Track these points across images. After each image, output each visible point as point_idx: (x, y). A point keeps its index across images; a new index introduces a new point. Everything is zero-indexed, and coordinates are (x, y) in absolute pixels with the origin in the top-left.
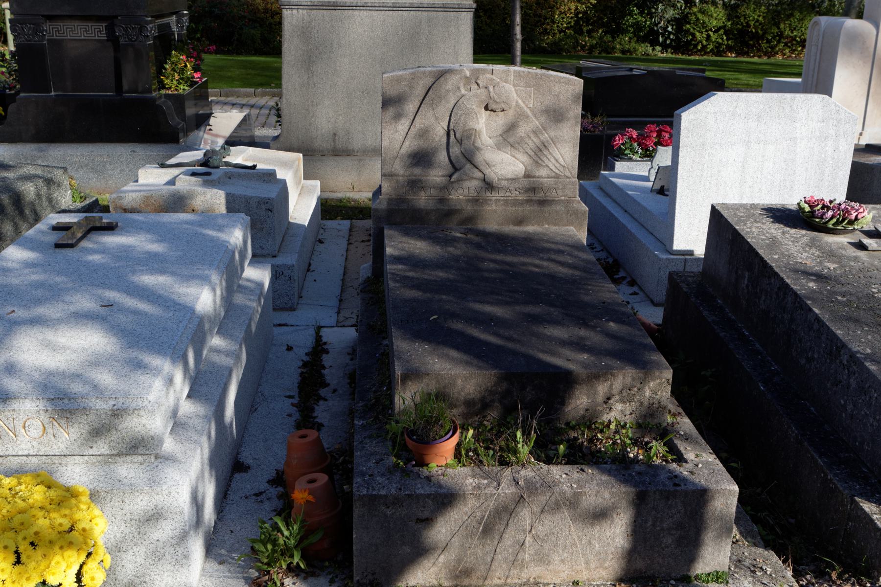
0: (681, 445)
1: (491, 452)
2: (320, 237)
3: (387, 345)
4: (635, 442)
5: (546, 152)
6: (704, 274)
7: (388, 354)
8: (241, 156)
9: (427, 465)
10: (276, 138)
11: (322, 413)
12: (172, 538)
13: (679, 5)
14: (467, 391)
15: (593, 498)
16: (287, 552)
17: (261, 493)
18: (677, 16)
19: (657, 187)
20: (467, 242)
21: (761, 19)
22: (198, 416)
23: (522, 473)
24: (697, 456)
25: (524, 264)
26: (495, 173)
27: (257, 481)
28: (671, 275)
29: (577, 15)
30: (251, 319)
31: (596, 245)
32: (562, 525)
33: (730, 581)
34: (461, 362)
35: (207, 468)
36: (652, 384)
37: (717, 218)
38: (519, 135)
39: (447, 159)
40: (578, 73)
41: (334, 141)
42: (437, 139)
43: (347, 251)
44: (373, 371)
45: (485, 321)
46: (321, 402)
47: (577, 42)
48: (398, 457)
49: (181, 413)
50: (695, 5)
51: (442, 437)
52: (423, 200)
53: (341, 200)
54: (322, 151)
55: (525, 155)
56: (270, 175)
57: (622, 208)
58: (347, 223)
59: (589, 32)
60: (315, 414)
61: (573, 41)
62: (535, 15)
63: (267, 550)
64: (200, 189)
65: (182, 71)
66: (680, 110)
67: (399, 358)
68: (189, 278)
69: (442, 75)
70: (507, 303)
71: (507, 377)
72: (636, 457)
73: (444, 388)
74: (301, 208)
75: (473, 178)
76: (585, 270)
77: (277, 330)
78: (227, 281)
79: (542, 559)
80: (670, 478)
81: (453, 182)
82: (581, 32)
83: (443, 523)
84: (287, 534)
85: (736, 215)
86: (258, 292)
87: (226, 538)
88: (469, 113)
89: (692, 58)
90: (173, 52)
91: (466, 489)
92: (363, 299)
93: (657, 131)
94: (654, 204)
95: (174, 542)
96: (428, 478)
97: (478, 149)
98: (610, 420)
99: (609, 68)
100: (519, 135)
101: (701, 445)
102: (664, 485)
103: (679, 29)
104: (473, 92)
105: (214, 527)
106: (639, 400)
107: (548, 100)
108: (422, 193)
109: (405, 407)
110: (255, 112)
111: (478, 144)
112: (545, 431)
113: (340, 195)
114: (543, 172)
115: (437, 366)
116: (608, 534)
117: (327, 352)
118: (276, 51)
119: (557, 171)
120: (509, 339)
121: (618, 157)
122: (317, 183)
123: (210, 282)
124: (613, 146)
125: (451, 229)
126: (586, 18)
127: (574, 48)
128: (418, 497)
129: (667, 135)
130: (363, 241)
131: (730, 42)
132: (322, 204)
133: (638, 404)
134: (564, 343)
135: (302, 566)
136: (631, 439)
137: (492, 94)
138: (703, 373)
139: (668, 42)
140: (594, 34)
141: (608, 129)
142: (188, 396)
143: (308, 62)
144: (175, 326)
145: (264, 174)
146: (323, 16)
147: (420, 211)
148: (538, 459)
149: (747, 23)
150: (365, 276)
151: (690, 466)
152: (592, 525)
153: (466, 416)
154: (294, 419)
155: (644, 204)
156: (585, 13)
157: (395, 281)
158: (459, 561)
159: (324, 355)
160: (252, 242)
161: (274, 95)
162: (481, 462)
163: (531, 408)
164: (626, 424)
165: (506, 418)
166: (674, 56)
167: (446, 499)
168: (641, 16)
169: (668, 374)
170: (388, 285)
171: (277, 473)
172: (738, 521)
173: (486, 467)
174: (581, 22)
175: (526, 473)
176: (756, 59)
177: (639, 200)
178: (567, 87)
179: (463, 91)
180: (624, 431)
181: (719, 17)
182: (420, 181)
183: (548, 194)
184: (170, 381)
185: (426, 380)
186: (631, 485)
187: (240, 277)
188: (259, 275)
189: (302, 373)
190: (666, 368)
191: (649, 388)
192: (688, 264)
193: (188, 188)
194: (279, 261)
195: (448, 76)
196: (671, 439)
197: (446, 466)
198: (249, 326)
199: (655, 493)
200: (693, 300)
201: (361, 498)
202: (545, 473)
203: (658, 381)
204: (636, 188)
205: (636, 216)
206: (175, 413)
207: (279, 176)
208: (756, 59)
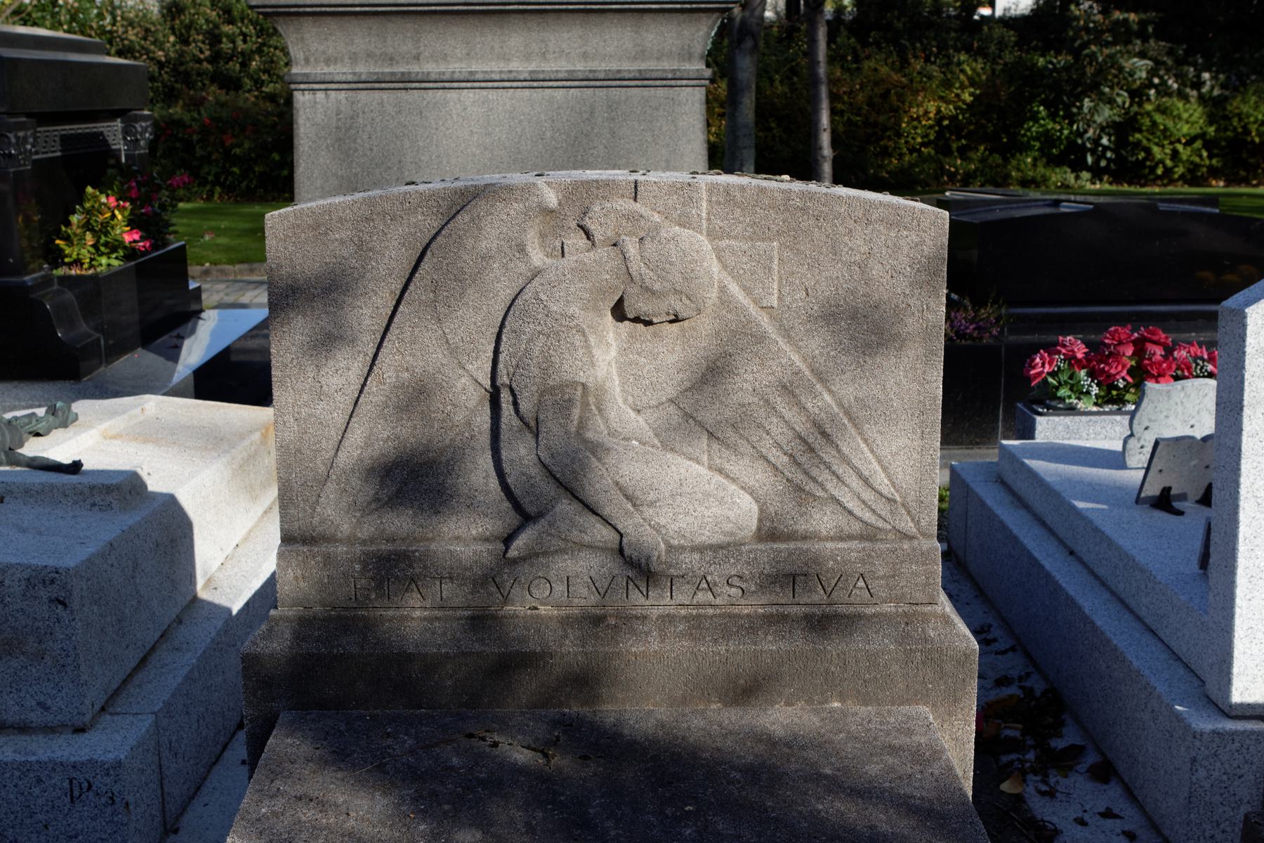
5: (828, 455)
13: (1119, 100)
18: (1117, 119)
19: (1152, 490)
26: (657, 528)
29: (939, 121)
31: (996, 632)
38: (736, 398)
39: (494, 483)
40: (941, 204)
42: (459, 417)
50: (1148, 100)
52: (415, 617)
55: (760, 465)
56: (125, 489)
57: (1061, 542)
59: (963, 152)
61: (934, 166)
65: (105, 228)
69: (463, 202)
75: (583, 546)
81: (514, 562)
82: (947, 151)
93: (1135, 342)
94: (1159, 547)
97: (596, 449)
100: (736, 398)
103: (1121, 142)
104: (570, 259)
107: (829, 279)
108: (414, 599)
111: (597, 430)
114: (823, 521)
119: (867, 516)
121: (1041, 403)
124: (1029, 379)
126: (956, 127)
131: (1214, 162)
137: (636, 266)
139: (1103, 163)
140: (972, 155)
141: (1011, 332)
146: (381, 103)
147: (404, 658)
149: (1245, 127)
155: (1124, 542)
156: (953, 119)
166: (1114, 188)
168: (1055, 122)
174: (946, 135)
181: (1193, 119)
183: (839, 595)
195: (482, 206)
204: (1094, 491)
205: (1101, 572)
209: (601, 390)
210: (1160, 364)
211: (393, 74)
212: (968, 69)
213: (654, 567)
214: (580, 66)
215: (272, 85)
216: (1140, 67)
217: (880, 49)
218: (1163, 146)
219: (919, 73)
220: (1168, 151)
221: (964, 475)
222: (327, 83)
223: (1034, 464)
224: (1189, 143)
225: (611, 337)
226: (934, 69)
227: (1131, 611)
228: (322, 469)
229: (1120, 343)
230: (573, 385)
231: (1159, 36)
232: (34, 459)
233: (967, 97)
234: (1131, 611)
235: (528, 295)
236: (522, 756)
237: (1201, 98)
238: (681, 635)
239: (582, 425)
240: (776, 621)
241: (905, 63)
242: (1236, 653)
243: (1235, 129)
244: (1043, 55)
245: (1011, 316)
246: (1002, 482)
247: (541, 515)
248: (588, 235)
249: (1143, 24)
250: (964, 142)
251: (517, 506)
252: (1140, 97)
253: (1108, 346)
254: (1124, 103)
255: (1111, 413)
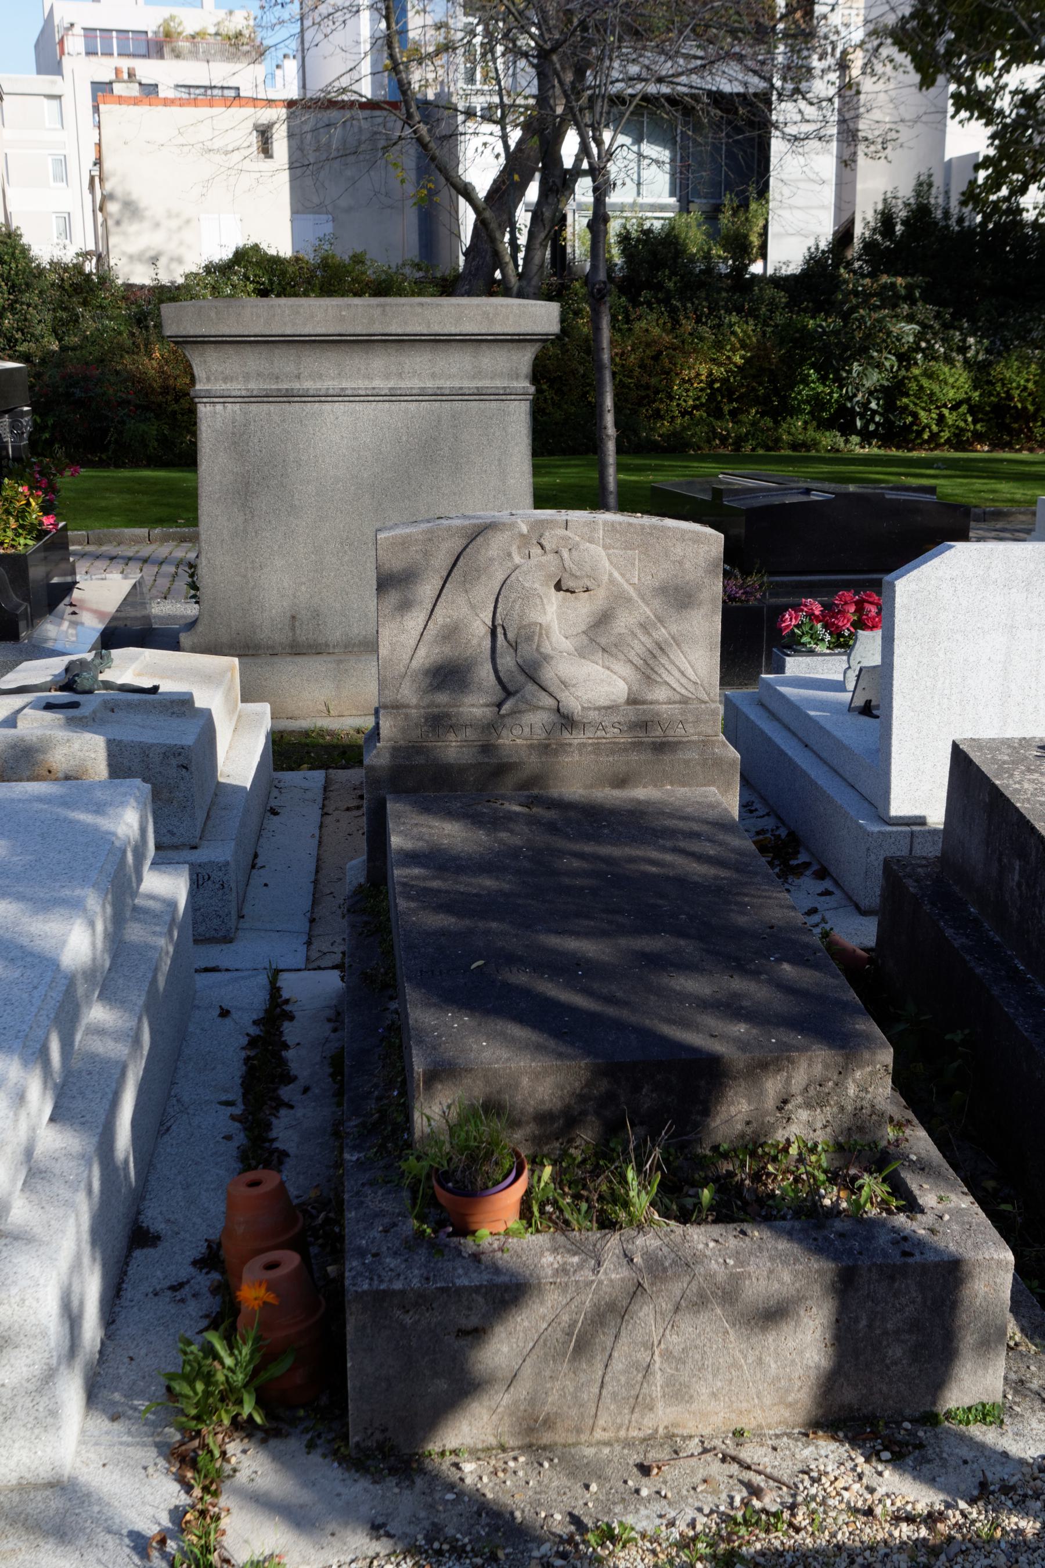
0: (913, 1182)
1: (584, 1206)
2: (273, 803)
3: (396, 1012)
4: (834, 1177)
5: (664, 660)
6: (943, 860)
7: (399, 1028)
8: (131, 667)
9: (473, 1233)
10: (191, 625)
11: (285, 1132)
12: (28, 1380)
13: (887, 364)
14: (538, 1096)
15: (763, 1282)
16: (230, 1395)
17: (181, 1285)
18: (886, 383)
19: (859, 702)
20: (533, 821)
21: (1030, 385)
22: (69, 1155)
23: (640, 1241)
24: (941, 1199)
25: (632, 860)
26: (577, 698)
27: (174, 1260)
28: (887, 863)
30: (156, 970)
32: (710, 1334)
33: (1007, 1420)
34: (527, 1046)
35: (86, 1248)
36: (858, 1074)
37: (962, 763)
41: (293, 628)
42: (475, 642)
43: (321, 827)
44: (373, 1065)
45: (566, 968)
46: (283, 1112)
47: (714, 431)
48: (422, 1218)
49: (38, 1151)
50: (916, 364)
51: (497, 1183)
52: (454, 749)
53: (306, 734)
54: (273, 647)
55: (629, 666)
57: (800, 739)
58: (318, 776)
60: (273, 1134)
61: (706, 429)
62: (638, 386)
63: (196, 1393)
64: (61, 734)
65: (22, 514)
66: (893, 574)
67: (420, 1042)
68: (45, 905)
69: (479, 532)
70: (604, 934)
71: (610, 1070)
72: (836, 1204)
73: (499, 1092)
74: (239, 757)
75: (539, 708)
76: (738, 867)
77: (203, 980)
78: (114, 905)
79: (678, 1393)
80: (895, 1243)
81: (503, 716)
82: (718, 414)
83: (503, 1335)
84: (231, 1363)
85: (994, 760)
86: (167, 918)
87: (122, 1371)
88: (528, 597)
89: (915, 454)
90: (6, 481)
91: (542, 1274)
92: (353, 926)
93: (857, 603)
94: (853, 732)
95: (31, 1387)
96: (476, 1257)
97: (547, 658)
98: (788, 1140)
99: (769, 489)
101: (946, 1179)
102: (885, 1254)
104: (534, 561)
105: (100, 1352)
106: (837, 1103)
108: (451, 737)
109: (432, 1131)
110: (150, 570)
111: (546, 649)
112: (676, 1164)
113: (304, 724)
114: (660, 694)
115: (487, 1055)
116: (791, 1344)
117: (291, 1017)
118: (189, 460)
119: (683, 691)
120: (610, 1000)
121: (789, 648)
122: (265, 708)
123: (85, 910)
124: (781, 630)
125: (503, 797)
126: (728, 390)
127: (709, 441)
128: (459, 1291)
129: (874, 610)
130: (348, 809)
131: (978, 426)
132: (274, 742)
133: (835, 1109)
134: (706, 1005)
135: (258, 1419)
136: (825, 1172)
137: (568, 563)
138: (948, 1037)
139: (872, 427)
140: (743, 417)
142: (52, 1119)
143: (243, 492)
144: (25, 996)
145: (172, 702)
146: (269, 414)
148: (666, 1214)
149: (1007, 392)
150: (355, 883)
151: (928, 1219)
152: (764, 1329)
153: (538, 1141)
154: (235, 1143)
155: (838, 734)
156: (725, 381)
157: (409, 898)
158: (532, 1401)
159: (286, 1024)
160: (155, 823)
161: (183, 539)
162: (567, 1223)
163: (652, 1125)
164: (816, 1145)
165: (608, 1141)
166: (882, 452)
167: (508, 1292)
168: (825, 385)
169: (886, 1056)
170: (396, 905)
171: (209, 1247)
172: (1016, 1307)
173: (576, 1233)
175: (647, 1242)
176: (1025, 455)
177: (828, 726)
178: (699, 545)
179: (517, 559)
180: (813, 1158)
182: (448, 715)
184: (20, 1098)
185: (468, 1081)
186: (828, 1257)
187: (135, 894)
188: (168, 886)
189: (248, 1059)
190: (882, 1046)
191: (854, 1081)
192: (916, 841)
193: (39, 732)
194: (203, 855)
195: (490, 533)
196: (895, 1170)
197: (507, 1233)
198: (154, 981)
199: (870, 1270)
200: (927, 908)
201: (360, 1296)
202: (679, 1240)
203: (869, 1069)
204: (822, 705)
205: (824, 755)
206: (29, 1153)
207: (200, 702)
208: (1025, 455)
209: (549, 627)
210: (874, 618)
211: (279, 390)
212: (739, 330)
213: (576, 718)
214: (430, 384)
215: (26, 344)
216: (908, 330)
217: (651, 309)
218: (930, 411)
219: (690, 334)
220: (934, 416)
221: (734, 700)
222: (225, 398)
223: (782, 689)
224: (955, 408)
225: (554, 599)
226: (705, 331)
227: (841, 776)
228: (403, 670)
229: (846, 603)
230: (536, 624)
231: (926, 300)
232: (123, 685)
233: (738, 359)
234: (841, 776)
235: (513, 577)
236: (517, 808)
237: (966, 361)
238: (590, 753)
239: (538, 646)
240: (637, 745)
241: (676, 323)
242: (893, 786)
243: (999, 394)
244: (813, 317)
245: (771, 583)
246: (762, 704)
247: (517, 692)
248: (542, 547)
249: (909, 287)
250: (735, 405)
251: (504, 687)
252: (908, 360)
253: (837, 605)
254: (892, 367)
255: (839, 654)
